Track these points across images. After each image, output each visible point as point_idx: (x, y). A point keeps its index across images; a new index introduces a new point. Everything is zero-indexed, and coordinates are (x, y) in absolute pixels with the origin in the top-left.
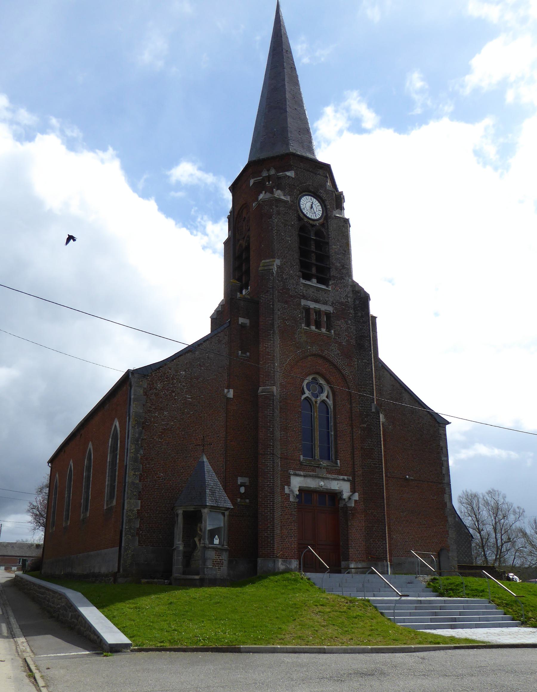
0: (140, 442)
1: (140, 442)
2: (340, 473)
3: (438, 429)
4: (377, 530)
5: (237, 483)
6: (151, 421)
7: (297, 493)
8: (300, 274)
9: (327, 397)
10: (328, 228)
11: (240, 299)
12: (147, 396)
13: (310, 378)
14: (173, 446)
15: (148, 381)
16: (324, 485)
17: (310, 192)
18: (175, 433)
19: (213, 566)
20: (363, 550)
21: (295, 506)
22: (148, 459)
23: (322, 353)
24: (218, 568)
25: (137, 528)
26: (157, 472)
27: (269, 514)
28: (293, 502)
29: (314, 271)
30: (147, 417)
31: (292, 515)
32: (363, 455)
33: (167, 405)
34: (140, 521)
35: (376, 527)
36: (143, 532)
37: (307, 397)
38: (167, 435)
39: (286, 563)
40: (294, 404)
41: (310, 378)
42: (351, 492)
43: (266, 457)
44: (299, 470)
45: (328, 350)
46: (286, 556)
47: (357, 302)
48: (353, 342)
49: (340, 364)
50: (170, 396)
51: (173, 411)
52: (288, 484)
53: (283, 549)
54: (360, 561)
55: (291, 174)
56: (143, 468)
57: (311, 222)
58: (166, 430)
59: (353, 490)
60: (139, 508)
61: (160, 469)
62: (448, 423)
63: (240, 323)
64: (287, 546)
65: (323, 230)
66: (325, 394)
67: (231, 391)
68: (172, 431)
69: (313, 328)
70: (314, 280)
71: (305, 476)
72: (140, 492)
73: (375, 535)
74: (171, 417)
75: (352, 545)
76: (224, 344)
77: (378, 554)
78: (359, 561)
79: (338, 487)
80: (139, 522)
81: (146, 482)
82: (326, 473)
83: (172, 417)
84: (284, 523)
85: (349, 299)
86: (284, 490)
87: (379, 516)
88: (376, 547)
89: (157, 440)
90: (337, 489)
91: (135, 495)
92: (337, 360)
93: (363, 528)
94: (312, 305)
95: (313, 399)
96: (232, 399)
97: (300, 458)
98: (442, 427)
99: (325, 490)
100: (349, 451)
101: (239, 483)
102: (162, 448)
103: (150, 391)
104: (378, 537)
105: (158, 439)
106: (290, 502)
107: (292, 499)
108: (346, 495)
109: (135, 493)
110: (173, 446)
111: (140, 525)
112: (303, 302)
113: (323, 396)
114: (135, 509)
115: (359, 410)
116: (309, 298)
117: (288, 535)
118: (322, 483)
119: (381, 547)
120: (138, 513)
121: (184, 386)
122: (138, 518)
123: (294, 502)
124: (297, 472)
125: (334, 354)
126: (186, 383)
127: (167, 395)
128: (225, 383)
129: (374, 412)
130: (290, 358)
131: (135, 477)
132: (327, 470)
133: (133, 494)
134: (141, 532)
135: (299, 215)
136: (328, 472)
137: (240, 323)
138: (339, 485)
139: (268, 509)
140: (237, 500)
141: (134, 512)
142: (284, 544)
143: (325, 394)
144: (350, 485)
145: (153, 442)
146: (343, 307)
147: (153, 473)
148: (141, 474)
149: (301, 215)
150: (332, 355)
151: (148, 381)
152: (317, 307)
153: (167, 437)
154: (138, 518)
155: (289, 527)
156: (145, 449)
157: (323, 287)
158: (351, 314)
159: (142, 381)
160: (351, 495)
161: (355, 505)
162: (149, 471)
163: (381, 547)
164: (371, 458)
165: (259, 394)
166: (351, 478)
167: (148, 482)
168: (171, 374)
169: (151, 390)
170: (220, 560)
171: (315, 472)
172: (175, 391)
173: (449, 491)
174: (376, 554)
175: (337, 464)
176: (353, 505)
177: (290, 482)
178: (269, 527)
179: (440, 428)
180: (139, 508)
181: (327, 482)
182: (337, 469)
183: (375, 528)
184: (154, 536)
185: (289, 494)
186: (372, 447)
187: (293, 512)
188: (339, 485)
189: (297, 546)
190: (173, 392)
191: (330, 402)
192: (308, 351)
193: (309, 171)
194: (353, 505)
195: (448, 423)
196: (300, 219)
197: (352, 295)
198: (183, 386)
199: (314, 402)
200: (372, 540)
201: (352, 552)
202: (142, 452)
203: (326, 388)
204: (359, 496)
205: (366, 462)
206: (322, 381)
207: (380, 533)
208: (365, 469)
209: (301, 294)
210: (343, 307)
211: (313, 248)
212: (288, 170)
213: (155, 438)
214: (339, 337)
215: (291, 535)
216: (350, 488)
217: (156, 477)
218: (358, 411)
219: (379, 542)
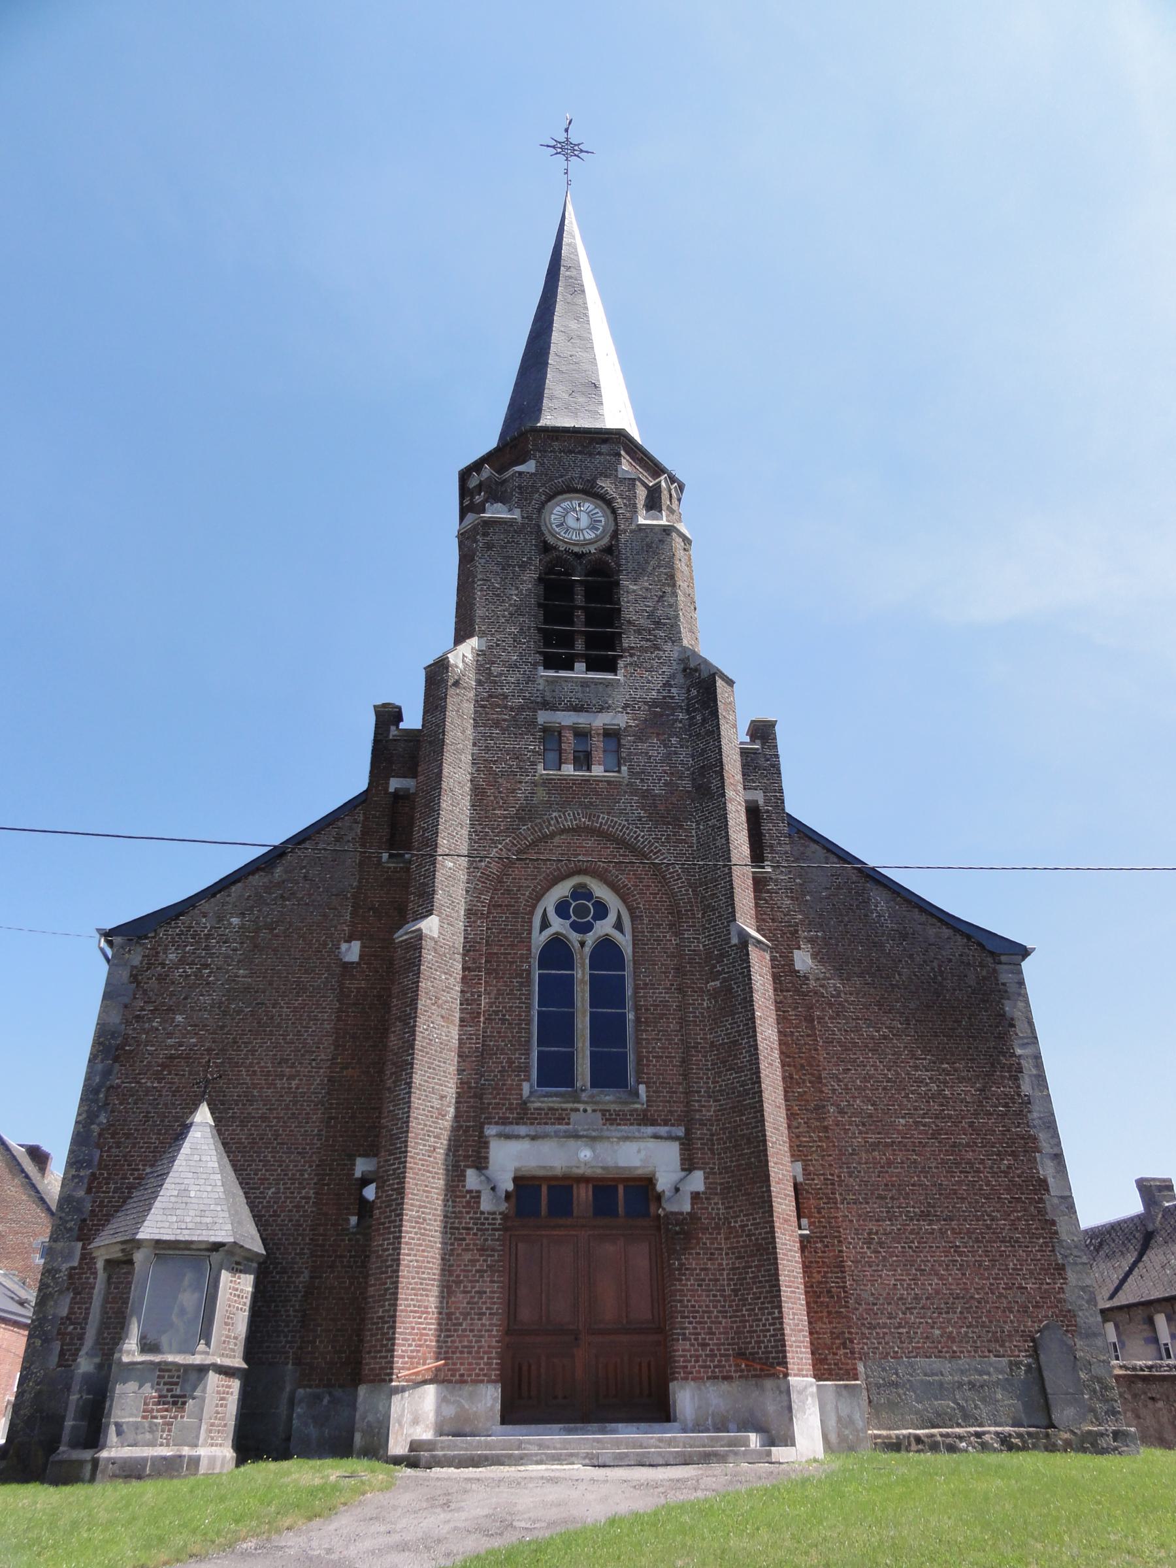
0: (101, 1096)
1: (101, 1096)
2: (646, 1119)
3: (995, 970)
4: (758, 1277)
5: (354, 1174)
6: (138, 1041)
7: (510, 1186)
8: (539, 658)
9: (619, 926)
10: (617, 556)
11: (395, 740)
12: (138, 983)
13: (562, 890)
14: (188, 1096)
15: (147, 949)
16: (596, 1157)
17: (576, 491)
18: (199, 1063)
19: (144, 1417)
20: (723, 1344)
21: (495, 1224)
22: (119, 1133)
23: (593, 821)
24: (165, 1424)
25: (62, 1318)
26: (138, 1165)
27: (391, 1252)
28: (488, 1213)
29: (580, 646)
30: (130, 1032)
31: (487, 1250)
32: (717, 1064)
33: (185, 998)
34: (73, 1298)
35: (756, 1266)
36: (75, 1329)
37: (557, 933)
38: (175, 1070)
39: (460, 1396)
40: (510, 954)
41: (562, 890)
42: (683, 1170)
43: (395, 1096)
44: (519, 1121)
45: (609, 813)
46: (462, 1375)
47: (694, 692)
48: (686, 784)
49: (643, 842)
50: (196, 976)
51: (200, 1010)
52: (480, 1163)
53: (453, 1353)
54: (716, 1378)
55: (529, 467)
56: (101, 1156)
57: (576, 549)
58: (175, 1058)
59: (688, 1165)
60: (76, 1264)
61: (146, 1156)
62: (1024, 952)
63: (391, 790)
64: (466, 1344)
65: (608, 558)
66: (612, 918)
67: (356, 946)
68: (190, 1058)
69: (568, 769)
70: (580, 666)
71: (533, 1138)
72: (84, 1220)
73: (753, 1294)
74: (191, 1026)
75: (685, 1328)
76: (349, 841)
77: (763, 1353)
78: (708, 1378)
79: (641, 1160)
80: (68, 1300)
81: (103, 1192)
82: (601, 1122)
83: (196, 1026)
84: (458, 1276)
85: (673, 690)
86: (464, 1181)
87: (760, 1234)
88: (756, 1331)
89: (149, 1084)
90: (637, 1163)
91: (71, 1229)
92: (635, 832)
93: (722, 1275)
94: (567, 719)
95: (574, 937)
96: (358, 963)
97: (522, 1090)
98: (1005, 964)
99: (599, 1171)
100: (675, 1057)
101: (358, 1174)
102: (158, 1104)
103: (147, 971)
104: (760, 1298)
105: (152, 1082)
106: (482, 1213)
107: (486, 1205)
108: (664, 1183)
109: (70, 1225)
110: (188, 1096)
111: (71, 1308)
112: (543, 717)
113: (604, 927)
114: (65, 1267)
115: (704, 946)
116: (560, 704)
117: (471, 1308)
118: (585, 1154)
119: (769, 1330)
120: (70, 1276)
121: (235, 950)
122: (68, 1289)
123: (494, 1213)
124: (508, 1129)
125: (626, 820)
126: (242, 943)
127: (190, 976)
128: (344, 930)
129: (735, 945)
130: (500, 846)
131: (78, 1183)
132: (604, 1115)
133: (65, 1228)
134: (72, 1327)
135: (545, 542)
136: (607, 1120)
137: (391, 790)
138: (643, 1153)
139: (389, 1239)
140: (349, 1220)
141: (62, 1274)
142: (458, 1336)
143: (612, 918)
144: (681, 1149)
145: (138, 1091)
146: (658, 709)
147: (126, 1167)
148: (93, 1174)
149: (551, 540)
150: (620, 824)
151: (147, 949)
152: (580, 721)
153: (176, 1075)
154: (68, 1289)
155: (473, 1287)
156: (112, 1111)
157: (610, 676)
158: (681, 722)
159: (130, 950)
160: (681, 1180)
161: (693, 1208)
162: (115, 1165)
163: (769, 1330)
164: (734, 1069)
165: (397, 941)
166: (680, 1131)
167: (109, 1192)
168: (206, 927)
169: (148, 969)
170: (172, 1396)
171: (568, 1124)
172: (210, 965)
173: (1053, 1142)
174: (758, 1353)
175: (637, 1094)
176: (687, 1208)
177: (487, 1158)
178: (389, 1289)
179: (998, 967)
180: (76, 1264)
181: (601, 1147)
182: (636, 1110)
183: (752, 1272)
184: (105, 1335)
185: (479, 1192)
186: (735, 1036)
187: (489, 1242)
188: (643, 1153)
189: (497, 1341)
190: (206, 966)
191: (625, 941)
192: (552, 822)
193: (571, 452)
194: (687, 1208)
195: (1024, 952)
196: (546, 548)
197: (682, 681)
198: (233, 950)
199: (577, 945)
200: (747, 1310)
201: (684, 1350)
202: (103, 1119)
203: (614, 903)
204: (706, 1178)
205: (724, 1081)
206: (601, 891)
207: (765, 1287)
208: (720, 1100)
209: (539, 700)
210: (658, 709)
211: (579, 599)
212: (523, 462)
213: (143, 1081)
214: (642, 780)
215: (481, 1308)
216: (681, 1159)
217: (134, 1179)
218: (701, 948)
219: (763, 1314)
